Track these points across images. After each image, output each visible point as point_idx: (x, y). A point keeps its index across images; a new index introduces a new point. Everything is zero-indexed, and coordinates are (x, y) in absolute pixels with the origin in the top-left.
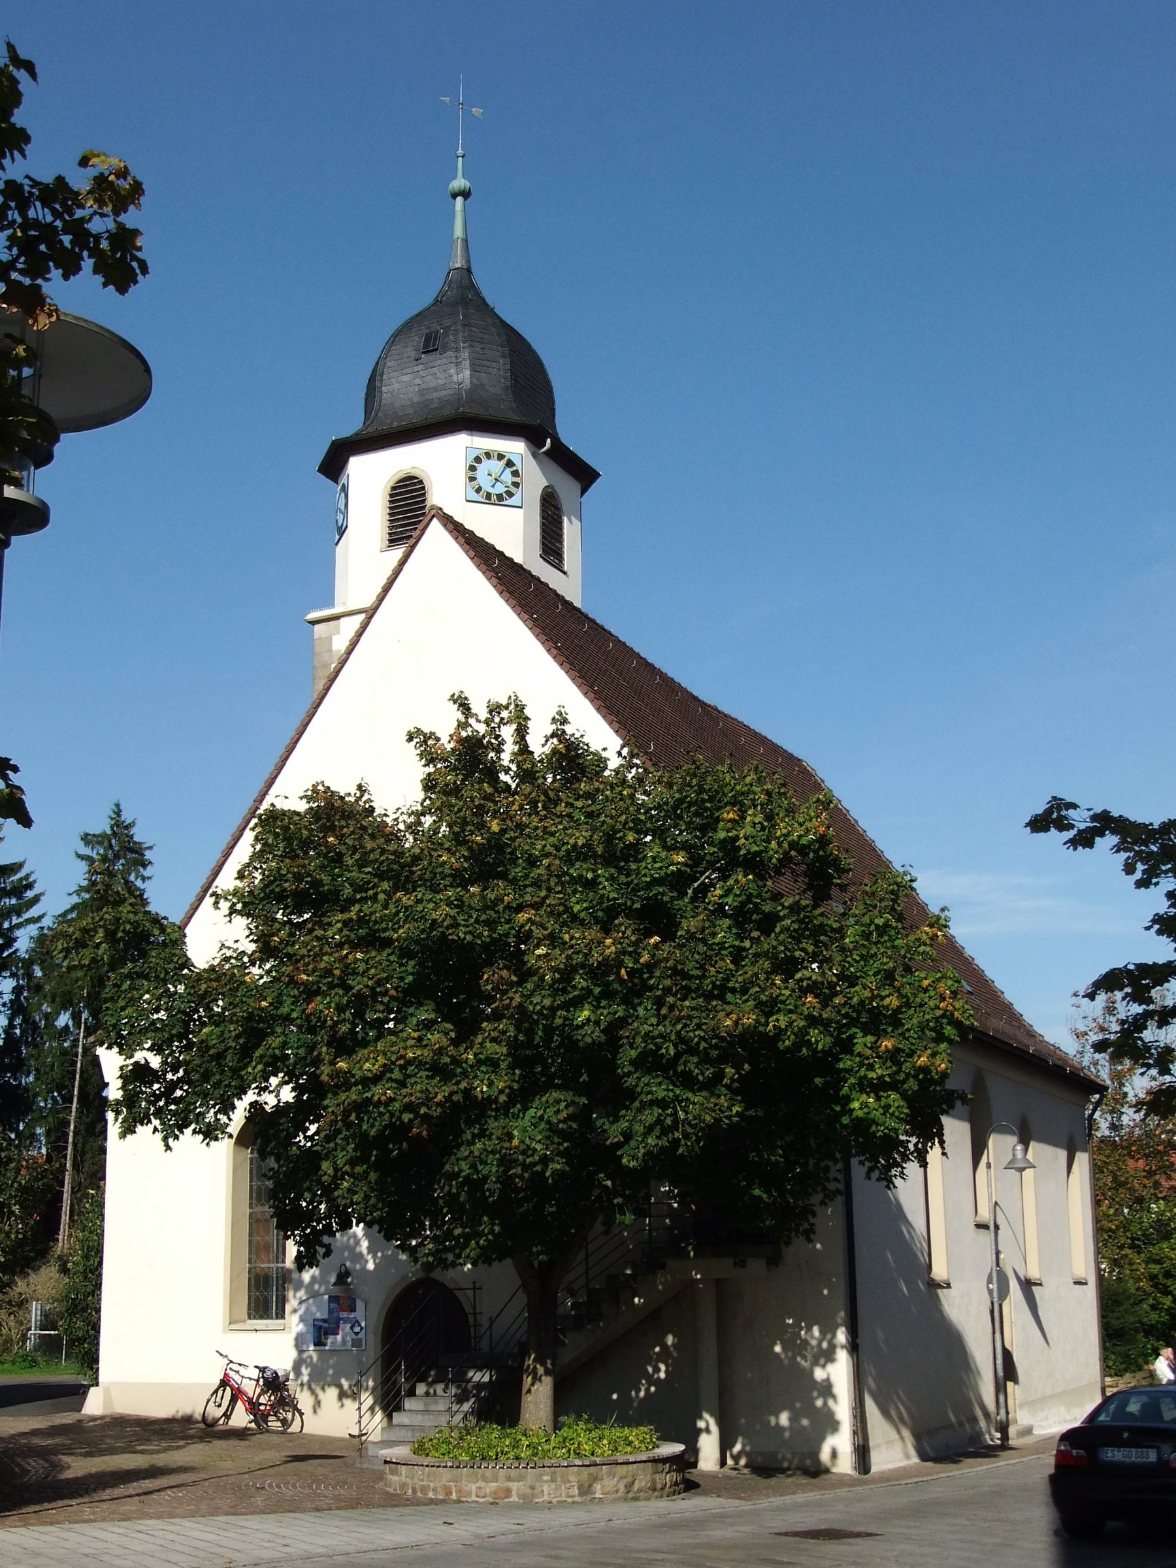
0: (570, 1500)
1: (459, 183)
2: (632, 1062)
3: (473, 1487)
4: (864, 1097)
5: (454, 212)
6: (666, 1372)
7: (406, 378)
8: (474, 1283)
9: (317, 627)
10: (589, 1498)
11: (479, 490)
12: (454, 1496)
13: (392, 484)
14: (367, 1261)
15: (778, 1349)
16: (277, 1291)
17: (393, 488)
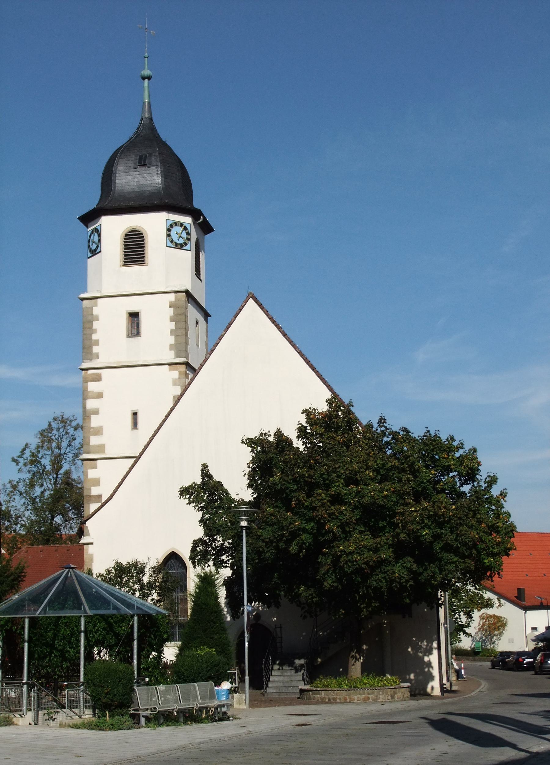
0: (388, 701)
1: (147, 72)
2: (440, 548)
3: (356, 697)
4: (489, 559)
5: (144, 87)
6: (363, 659)
7: (129, 177)
8: (276, 625)
9: (84, 302)
10: (394, 700)
11: (172, 241)
12: (348, 701)
13: (125, 233)
14: (227, 617)
15: (410, 650)
16: (178, 630)
17: (126, 235)
